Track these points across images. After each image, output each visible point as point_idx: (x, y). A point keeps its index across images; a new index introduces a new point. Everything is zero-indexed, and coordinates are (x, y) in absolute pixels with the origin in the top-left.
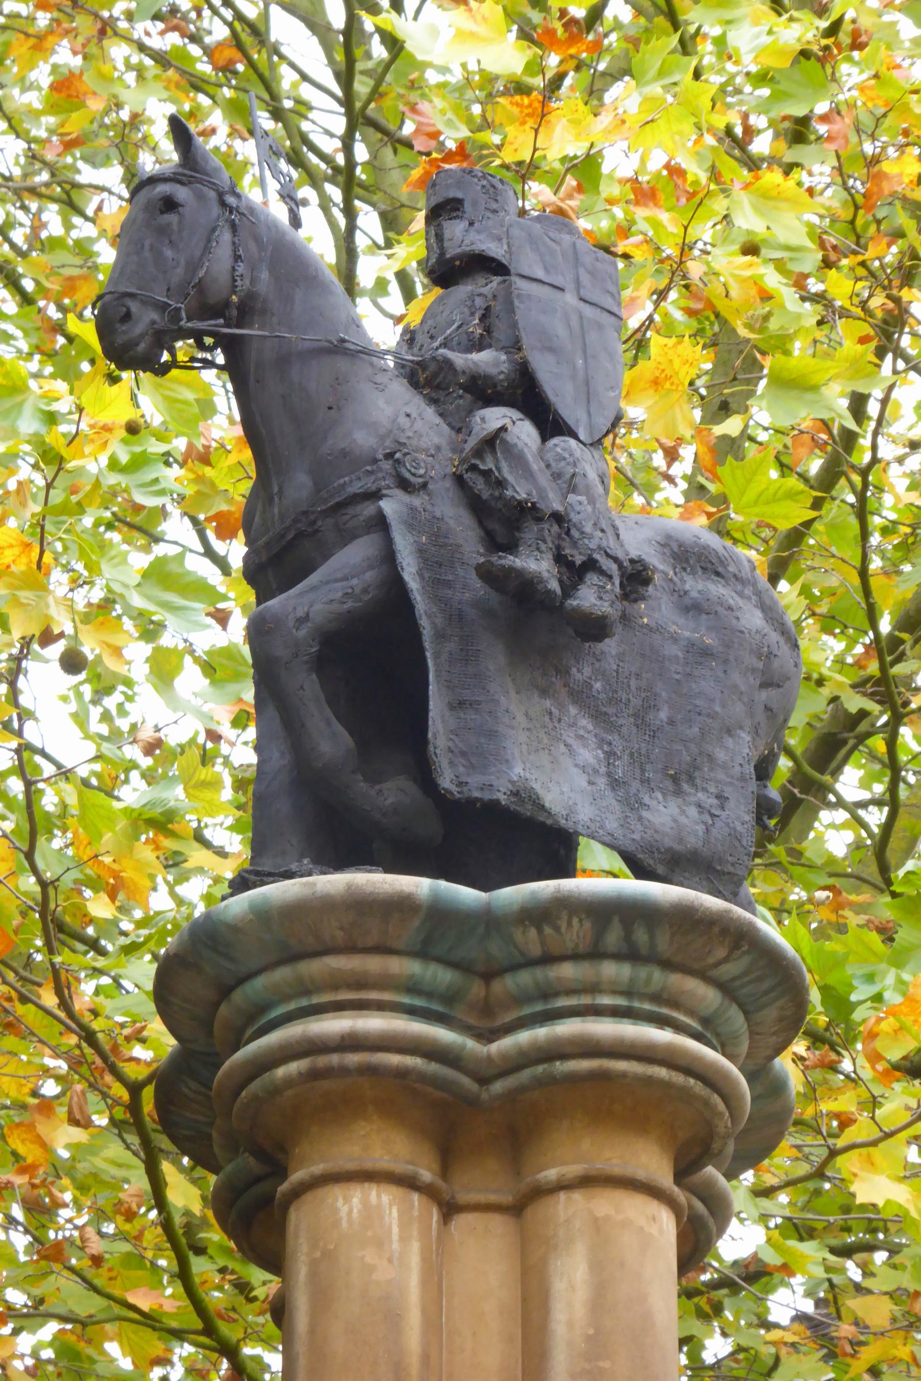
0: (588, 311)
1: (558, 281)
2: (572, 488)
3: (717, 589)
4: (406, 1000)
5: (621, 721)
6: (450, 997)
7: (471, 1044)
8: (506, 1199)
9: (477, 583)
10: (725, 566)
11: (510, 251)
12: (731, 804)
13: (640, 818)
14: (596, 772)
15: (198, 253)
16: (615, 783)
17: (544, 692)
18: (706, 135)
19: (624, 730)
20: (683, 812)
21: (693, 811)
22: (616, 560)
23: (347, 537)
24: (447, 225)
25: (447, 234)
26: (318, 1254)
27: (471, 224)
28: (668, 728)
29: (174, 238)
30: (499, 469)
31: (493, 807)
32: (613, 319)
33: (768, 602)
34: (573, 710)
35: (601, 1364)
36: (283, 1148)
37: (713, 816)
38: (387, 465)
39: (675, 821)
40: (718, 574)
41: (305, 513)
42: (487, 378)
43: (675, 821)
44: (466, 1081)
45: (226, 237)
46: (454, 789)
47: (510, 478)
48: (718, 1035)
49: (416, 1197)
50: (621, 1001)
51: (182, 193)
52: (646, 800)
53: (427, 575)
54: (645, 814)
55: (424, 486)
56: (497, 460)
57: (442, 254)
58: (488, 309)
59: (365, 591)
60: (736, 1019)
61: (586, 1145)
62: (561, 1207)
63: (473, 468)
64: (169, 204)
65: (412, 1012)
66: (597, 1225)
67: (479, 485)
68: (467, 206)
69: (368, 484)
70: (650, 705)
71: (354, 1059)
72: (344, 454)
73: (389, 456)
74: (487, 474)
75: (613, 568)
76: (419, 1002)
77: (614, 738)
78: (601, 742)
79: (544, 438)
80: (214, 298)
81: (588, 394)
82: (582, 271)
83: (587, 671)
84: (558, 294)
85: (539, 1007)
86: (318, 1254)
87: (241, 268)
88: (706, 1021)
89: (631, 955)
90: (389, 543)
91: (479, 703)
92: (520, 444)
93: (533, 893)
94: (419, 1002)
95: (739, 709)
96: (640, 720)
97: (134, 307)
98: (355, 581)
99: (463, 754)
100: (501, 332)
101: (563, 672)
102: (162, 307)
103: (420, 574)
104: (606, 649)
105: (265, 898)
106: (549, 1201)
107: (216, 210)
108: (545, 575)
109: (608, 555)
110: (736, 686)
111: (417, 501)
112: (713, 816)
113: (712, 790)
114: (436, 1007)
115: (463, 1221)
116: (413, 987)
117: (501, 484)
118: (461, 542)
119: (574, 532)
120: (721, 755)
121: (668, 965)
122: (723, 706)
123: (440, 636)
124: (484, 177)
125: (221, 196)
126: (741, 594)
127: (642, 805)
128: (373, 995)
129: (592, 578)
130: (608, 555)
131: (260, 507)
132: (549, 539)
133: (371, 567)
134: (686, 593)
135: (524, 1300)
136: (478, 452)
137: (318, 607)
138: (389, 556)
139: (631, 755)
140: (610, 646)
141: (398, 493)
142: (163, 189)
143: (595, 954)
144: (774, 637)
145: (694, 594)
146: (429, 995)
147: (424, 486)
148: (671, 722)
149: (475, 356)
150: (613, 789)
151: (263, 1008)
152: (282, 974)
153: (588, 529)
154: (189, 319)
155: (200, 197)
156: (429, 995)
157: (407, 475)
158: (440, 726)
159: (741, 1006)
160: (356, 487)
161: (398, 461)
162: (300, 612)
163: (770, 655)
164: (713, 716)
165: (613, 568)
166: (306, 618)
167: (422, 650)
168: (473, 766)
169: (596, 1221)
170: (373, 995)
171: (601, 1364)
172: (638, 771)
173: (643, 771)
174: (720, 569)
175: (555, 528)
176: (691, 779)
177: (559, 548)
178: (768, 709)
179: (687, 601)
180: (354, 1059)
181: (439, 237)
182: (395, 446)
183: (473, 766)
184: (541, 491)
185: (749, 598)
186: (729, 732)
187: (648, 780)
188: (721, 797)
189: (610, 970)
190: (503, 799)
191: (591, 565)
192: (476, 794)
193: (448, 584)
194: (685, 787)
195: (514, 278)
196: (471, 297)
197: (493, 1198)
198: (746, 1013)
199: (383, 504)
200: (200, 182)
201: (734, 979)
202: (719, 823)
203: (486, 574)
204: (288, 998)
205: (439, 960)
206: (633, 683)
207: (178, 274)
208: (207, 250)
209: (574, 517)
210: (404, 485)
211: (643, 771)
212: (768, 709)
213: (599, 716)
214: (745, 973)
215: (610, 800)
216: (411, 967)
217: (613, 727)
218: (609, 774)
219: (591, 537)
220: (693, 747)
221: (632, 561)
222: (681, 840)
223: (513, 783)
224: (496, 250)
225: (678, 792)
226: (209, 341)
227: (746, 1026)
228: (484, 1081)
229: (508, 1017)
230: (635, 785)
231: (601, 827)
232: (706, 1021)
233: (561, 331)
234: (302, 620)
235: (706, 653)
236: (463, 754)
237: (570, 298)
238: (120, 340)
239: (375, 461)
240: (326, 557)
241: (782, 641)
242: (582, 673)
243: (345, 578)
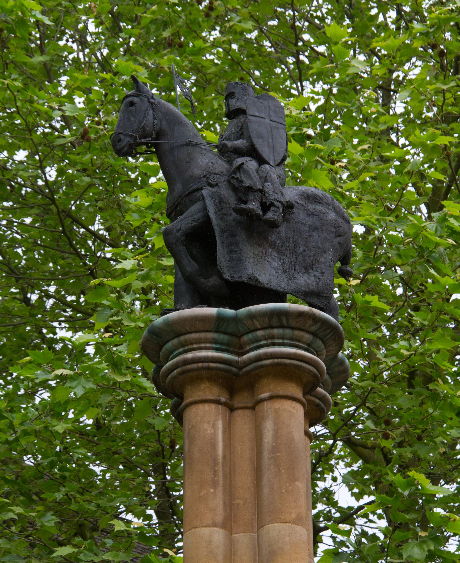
0: (274, 124)
1: (263, 115)
2: (266, 181)
3: (319, 208)
4: (214, 346)
5: (287, 252)
6: (227, 345)
7: (236, 358)
8: (250, 405)
9: (235, 214)
10: (322, 200)
11: (247, 108)
12: (326, 275)
13: (294, 282)
14: (278, 269)
15: (142, 118)
16: (285, 272)
17: (260, 246)
19: (288, 255)
20: (309, 279)
21: (312, 278)
22: (280, 202)
23: (194, 203)
24: (230, 101)
25: (230, 104)
26: (190, 427)
27: (238, 100)
28: (303, 253)
29: (134, 114)
30: (241, 177)
31: (243, 283)
32: (282, 126)
33: (338, 210)
34: (270, 250)
35: (278, 454)
36: (183, 394)
37: (319, 279)
38: (204, 179)
39: (306, 282)
40: (320, 203)
41: (180, 196)
42: (239, 148)
43: (306, 282)
44: (234, 369)
45: (151, 112)
46: (230, 278)
47: (244, 179)
48: (314, 349)
49: (220, 406)
50: (281, 341)
51: (136, 100)
52: (296, 276)
53: (218, 212)
54: (295, 280)
55: (217, 184)
56: (240, 174)
57: (229, 110)
58: (242, 126)
59: (198, 219)
60: (319, 343)
61: (272, 386)
62: (265, 406)
63: (233, 177)
64: (132, 104)
65: (216, 349)
66: (276, 411)
67: (235, 182)
68: (236, 95)
69: (199, 185)
71: (194, 366)
72: (191, 177)
73: (205, 176)
74: (237, 179)
75: (279, 205)
76: (218, 346)
77: (285, 258)
79: (260, 165)
81: (274, 150)
82: (271, 111)
83: (274, 237)
84: (263, 120)
85: (255, 345)
86: (190, 427)
87: (156, 122)
88: (309, 345)
89: (282, 326)
90: (205, 203)
91: (236, 251)
92: (248, 169)
93: (249, 310)
94: (218, 346)
95: (328, 245)
96: (294, 251)
97: (122, 136)
98: (195, 216)
99: (232, 267)
101: (266, 239)
102: (131, 136)
103: (215, 212)
104: (280, 230)
105: (249, 310)
106: (261, 405)
107: (147, 104)
108: (256, 209)
109: (277, 201)
110: (326, 237)
111: (214, 190)
112: (319, 279)
113: (319, 271)
114: (224, 347)
117: (242, 182)
118: (229, 201)
119: (267, 195)
120: (322, 260)
121: (293, 328)
122: (322, 244)
123: (223, 231)
124: (242, 84)
125: (148, 99)
126: (328, 209)
127: (295, 278)
128: (203, 345)
129: (273, 209)
130: (277, 201)
132: (257, 198)
133: (200, 212)
134: (309, 210)
136: (234, 172)
138: (205, 208)
139: (291, 262)
140: (282, 229)
141: (208, 188)
142: (130, 99)
144: (340, 221)
145: (311, 210)
146: (222, 344)
147: (217, 184)
148: (304, 251)
149: (236, 142)
150: (285, 274)
152: (175, 341)
153: (271, 193)
154: (140, 139)
155: (142, 100)
156: (222, 344)
157: (211, 182)
158: (223, 260)
159: (321, 339)
160: (195, 187)
161: (208, 178)
162: (178, 228)
163: (338, 227)
164: (319, 248)
165: (279, 205)
166: (180, 229)
167: (214, 236)
168: (235, 271)
169: (275, 409)
171: (278, 454)
172: (293, 267)
173: (295, 267)
174: (321, 201)
175: (260, 194)
176: (312, 268)
177: (261, 200)
178: (339, 243)
179: (310, 212)
180: (194, 366)
182: (207, 173)
183: (235, 271)
184: (255, 183)
185: (331, 209)
186: (325, 252)
187: (297, 270)
188: (322, 273)
189: (276, 331)
190: (245, 280)
191: (272, 204)
192: (237, 280)
193: (226, 215)
194: (310, 271)
196: (237, 123)
197: (246, 405)
198: (323, 342)
200: (142, 95)
201: (316, 331)
202: (321, 281)
203: (238, 211)
204: (178, 348)
205: (225, 333)
206: (291, 240)
207: (135, 126)
208: (144, 117)
209: (266, 190)
210: (211, 185)
211: (295, 267)
212: (339, 243)
213: (280, 252)
214: (319, 329)
215: (284, 277)
217: (284, 254)
218: (283, 269)
219: (271, 195)
220: (312, 258)
221: (287, 202)
222: (308, 288)
223: (248, 275)
224: (244, 107)
225: (307, 273)
227: (323, 345)
228: (241, 369)
229: (248, 348)
230: (292, 272)
231: (280, 286)
232: (309, 345)
234: (178, 231)
235: (316, 228)
236: (232, 267)
237: (267, 121)
238: (118, 147)
239: (200, 178)
240: (187, 210)
241: (343, 222)
242: (272, 238)
243: (192, 216)
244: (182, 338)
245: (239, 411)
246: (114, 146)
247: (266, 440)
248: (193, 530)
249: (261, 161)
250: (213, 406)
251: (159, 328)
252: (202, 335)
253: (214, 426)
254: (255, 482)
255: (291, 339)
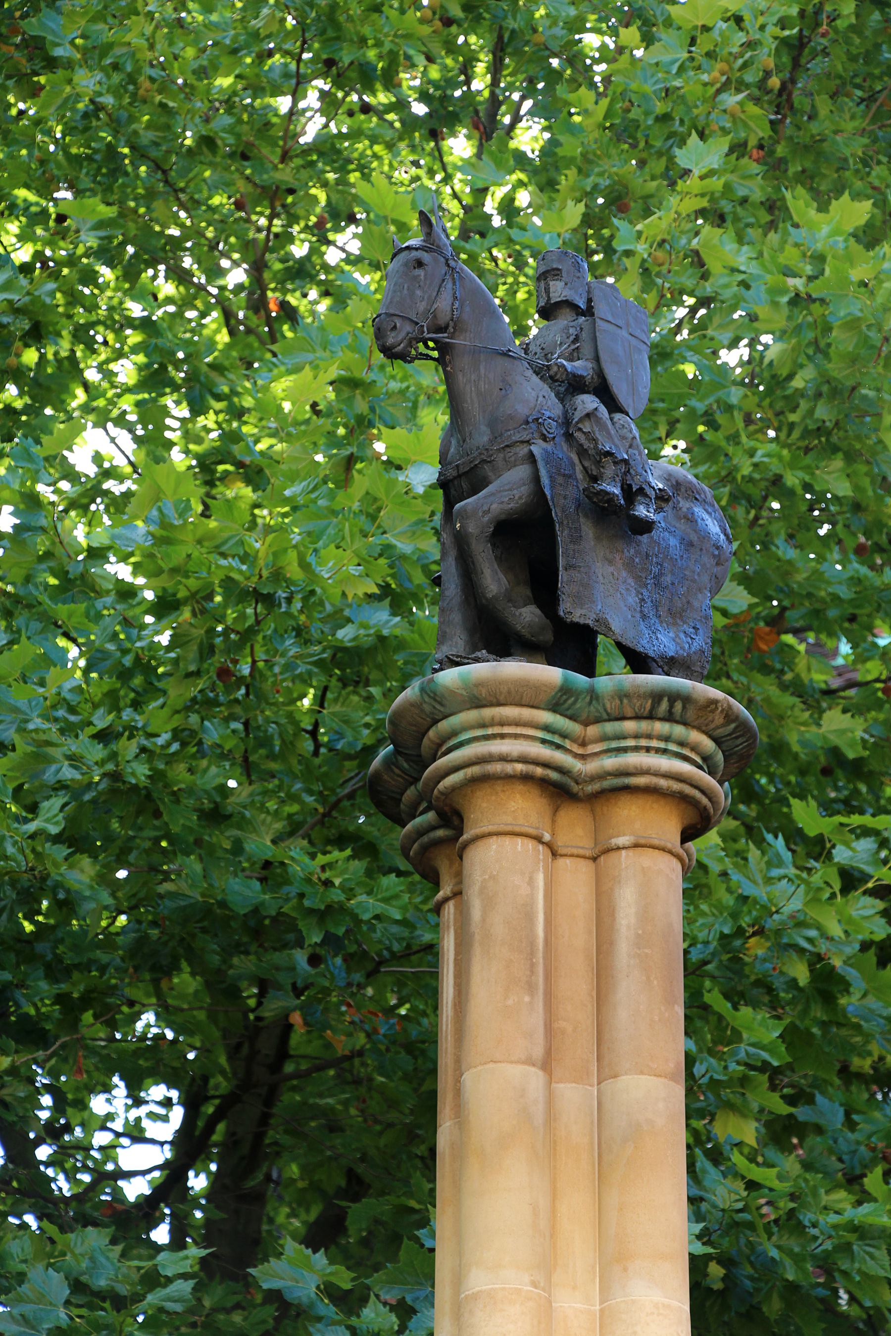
0: (634, 341)
1: (620, 323)
18: (788, 248)
49: (541, 847)
50: (662, 745)
51: (426, 257)
68: (564, 274)
70: (661, 574)
76: (548, 737)
78: (639, 593)
80: (442, 322)
83: (632, 551)
88: (705, 759)
89: (669, 718)
90: (536, 471)
94: (548, 737)
100: (587, 349)
106: (613, 855)
115: (562, 862)
116: (547, 728)
117: (595, 440)
131: (454, 442)
135: (598, 910)
137: (494, 506)
138: (536, 479)
143: (651, 717)
151: (454, 733)
152: (471, 715)
162: (485, 508)
164: (694, 581)
170: (506, 730)
176: (681, 617)
181: (547, 291)
191: (641, 491)
195: (598, 321)
196: (567, 328)
197: (581, 852)
199: (533, 448)
210: (544, 438)
216: (546, 717)
225: (675, 624)
226: (431, 344)
232: (705, 759)
233: (621, 353)
237: (624, 333)
244: (488, 713)
245: (568, 861)
246: (379, 334)
247: (624, 922)
248: (491, 1065)
249: (614, 406)
250: (530, 844)
251: (447, 688)
252: (526, 713)
253: (531, 882)
254: (594, 994)
255: (682, 744)
